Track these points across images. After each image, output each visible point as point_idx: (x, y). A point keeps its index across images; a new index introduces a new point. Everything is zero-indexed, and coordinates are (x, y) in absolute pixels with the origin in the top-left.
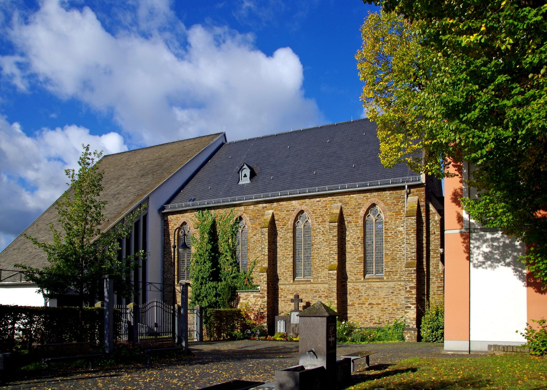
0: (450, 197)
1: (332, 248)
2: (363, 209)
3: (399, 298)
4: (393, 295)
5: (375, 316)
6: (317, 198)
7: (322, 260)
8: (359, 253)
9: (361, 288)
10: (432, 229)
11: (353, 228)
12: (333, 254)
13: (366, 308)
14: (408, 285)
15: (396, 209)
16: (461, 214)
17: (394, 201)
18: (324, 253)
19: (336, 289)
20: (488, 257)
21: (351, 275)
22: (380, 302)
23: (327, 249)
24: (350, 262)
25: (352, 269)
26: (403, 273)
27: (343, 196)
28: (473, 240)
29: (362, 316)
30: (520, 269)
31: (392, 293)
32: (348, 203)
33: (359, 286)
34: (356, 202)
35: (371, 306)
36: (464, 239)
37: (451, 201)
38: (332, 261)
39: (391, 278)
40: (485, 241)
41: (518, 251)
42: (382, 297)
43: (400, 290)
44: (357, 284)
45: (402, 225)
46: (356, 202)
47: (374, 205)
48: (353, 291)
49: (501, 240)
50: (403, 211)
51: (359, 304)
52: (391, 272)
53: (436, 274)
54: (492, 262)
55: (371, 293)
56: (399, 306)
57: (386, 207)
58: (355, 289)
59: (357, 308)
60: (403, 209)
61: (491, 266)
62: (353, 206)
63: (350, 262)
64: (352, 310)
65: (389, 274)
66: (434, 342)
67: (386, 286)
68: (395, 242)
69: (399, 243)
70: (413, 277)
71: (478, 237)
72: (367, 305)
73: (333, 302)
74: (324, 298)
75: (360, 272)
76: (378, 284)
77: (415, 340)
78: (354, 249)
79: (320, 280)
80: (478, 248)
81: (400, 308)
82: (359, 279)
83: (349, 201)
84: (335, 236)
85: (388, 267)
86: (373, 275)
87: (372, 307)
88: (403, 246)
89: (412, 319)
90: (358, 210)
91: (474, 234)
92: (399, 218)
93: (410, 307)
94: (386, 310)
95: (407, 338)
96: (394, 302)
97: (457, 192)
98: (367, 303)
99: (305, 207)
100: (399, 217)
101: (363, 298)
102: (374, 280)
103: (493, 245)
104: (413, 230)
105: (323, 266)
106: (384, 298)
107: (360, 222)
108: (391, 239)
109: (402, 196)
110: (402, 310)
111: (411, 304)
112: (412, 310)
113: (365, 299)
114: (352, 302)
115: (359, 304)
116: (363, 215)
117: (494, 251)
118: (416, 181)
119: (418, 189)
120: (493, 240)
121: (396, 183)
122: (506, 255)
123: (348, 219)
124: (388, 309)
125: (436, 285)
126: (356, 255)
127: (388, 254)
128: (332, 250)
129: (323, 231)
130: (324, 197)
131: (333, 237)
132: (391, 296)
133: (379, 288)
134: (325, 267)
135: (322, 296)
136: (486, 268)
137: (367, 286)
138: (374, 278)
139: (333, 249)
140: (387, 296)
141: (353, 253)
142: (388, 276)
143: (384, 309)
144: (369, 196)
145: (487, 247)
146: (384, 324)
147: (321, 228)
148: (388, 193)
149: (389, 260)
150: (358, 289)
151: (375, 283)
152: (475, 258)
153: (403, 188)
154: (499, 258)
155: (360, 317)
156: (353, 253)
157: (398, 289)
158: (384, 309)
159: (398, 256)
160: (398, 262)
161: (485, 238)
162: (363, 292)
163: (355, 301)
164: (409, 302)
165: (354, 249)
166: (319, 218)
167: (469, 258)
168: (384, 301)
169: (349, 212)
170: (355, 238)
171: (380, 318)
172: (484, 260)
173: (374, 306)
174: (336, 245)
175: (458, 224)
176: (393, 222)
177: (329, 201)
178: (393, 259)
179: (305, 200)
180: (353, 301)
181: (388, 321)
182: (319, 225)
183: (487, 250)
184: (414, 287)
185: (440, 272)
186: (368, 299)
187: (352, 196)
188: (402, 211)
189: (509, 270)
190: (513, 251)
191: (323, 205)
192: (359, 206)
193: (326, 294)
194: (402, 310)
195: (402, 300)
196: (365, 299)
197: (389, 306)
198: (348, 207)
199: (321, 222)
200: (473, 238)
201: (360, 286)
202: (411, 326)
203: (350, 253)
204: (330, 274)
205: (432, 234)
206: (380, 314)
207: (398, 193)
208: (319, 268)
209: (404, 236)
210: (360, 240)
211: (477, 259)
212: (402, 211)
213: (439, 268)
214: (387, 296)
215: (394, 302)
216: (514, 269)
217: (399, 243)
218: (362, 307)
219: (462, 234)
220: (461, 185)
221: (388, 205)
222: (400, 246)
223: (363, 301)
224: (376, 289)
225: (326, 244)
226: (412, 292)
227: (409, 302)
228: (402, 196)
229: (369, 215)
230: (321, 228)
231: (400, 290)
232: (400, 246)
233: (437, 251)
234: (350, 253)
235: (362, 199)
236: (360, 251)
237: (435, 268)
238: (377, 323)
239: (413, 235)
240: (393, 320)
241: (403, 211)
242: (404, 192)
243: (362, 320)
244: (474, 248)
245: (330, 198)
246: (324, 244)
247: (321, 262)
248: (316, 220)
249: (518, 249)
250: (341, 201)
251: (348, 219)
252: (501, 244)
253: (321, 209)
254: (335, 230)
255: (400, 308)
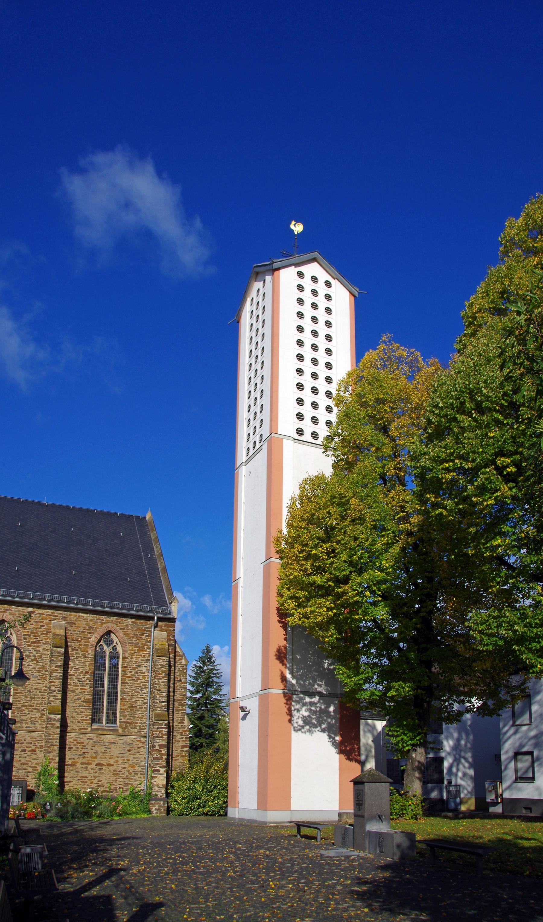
0: (274, 654)
1: (55, 682)
2: (96, 635)
3: (138, 758)
4: (130, 754)
5: (104, 781)
6: (28, 607)
7: (31, 698)
8: (86, 693)
9: (86, 741)
10: (178, 674)
11: (79, 659)
12: (55, 691)
13: (92, 769)
14: (157, 742)
15: (138, 643)
16: (284, 673)
17: (137, 633)
18: (35, 687)
19: (58, 741)
20: (307, 721)
21: (73, 722)
22: (112, 762)
23: (38, 681)
24: (73, 705)
25: (74, 714)
26: (143, 726)
27: (69, 613)
28: (294, 702)
29: (86, 780)
30: (333, 736)
31: (129, 751)
32: (75, 624)
33: (84, 738)
34: (87, 624)
35: (100, 767)
36: (287, 700)
37: (275, 657)
38: (53, 701)
39: (128, 731)
40: (304, 704)
41: (332, 718)
42: (115, 755)
43: (139, 748)
44: (81, 736)
45: (145, 664)
46: (87, 624)
47: (109, 633)
48: (75, 745)
49: (318, 705)
50: (147, 648)
51: (82, 764)
52: (128, 723)
53: (181, 731)
54: (310, 727)
55: (101, 749)
56: (137, 768)
57: (126, 639)
58: (77, 743)
59: (79, 770)
60: (147, 645)
61: (309, 731)
62: (82, 629)
63: (73, 705)
64: (72, 772)
65: (126, 726)
66: (187, 815)
67: (121, 741)
68: (135, 685)
69: (140, 687)
70: (164, 733)
71: (298, 699)
72: (93, 765)
73: (52, 759)
74: (29, 753)
75: (87, 720)
76: (110, 737)
77: (164, 815)
78: (80, 687)
79: (24, 725)
80: (298, 711)
81: (139, 772)
82: (84, 729)
83: (76, 620)
84: (60, 667)
85: (125, 717)
86: (102, 725)
87: (101, 769)
88: (145, 691)
89: (161, 786)
90: (89, 635)
91: (295, 696)
92: (141, 655)
93: (159, 771)
94: (120, 773)
95: (155, 812)
96: (130, 763)
97: (281, 649)
98: (94, 763)
99: (9, 617)
100: (141, 653)
101: (89, 755)
102: (105, 732)
103: (311, 710)
104: (164, 674)
105: (31, 706)
106: (118, 757)
107: (90, 651)
108: (130, 680)
109: (147, 628)
110: (141, 774)
111: (160, 767)
112: (160, 774)
113: (92, 757)
114: (73, 760)
115: (82, 764)
116: (95, 644)
117: (312, 716)
118: (166, 613)
119: (167, 623)
120: (312, 704)
121: (141, 611)
122: (322, 721)
123: (73, 645)
124: (123, 772)
125: (181, 743)
126: (81, 695)
127: (126, 699)
128: (53, 686)
129: (34, 656)
130: (7, 604)
131: (57, 666)
132: (127, 754)
133: (111, 743)
134: (35, 707)
135: (27, 749)
136: (305, 733)
137: (95, 739)
138: (104, 730)
139: (56, 684)
140: (121, 755)
141: (77, 692)
142: (125, 728)
143: (117, 771)
144: (105, 619)
145: (306, 711)
146: (117, 792)
147: (33, 651)
148: (130, 621)
149: (126, 707)
150: (83, 743)
151: (107, 736)
152: (295, 721)
153: (152, 618)
154: (316, 723)
155: (83, 782)
156: (77, 692)
157: (136, 746)
158: (117, 771)
159: (139, 704)
160: (138, 711)
161: (304, 701)
162: (89, 747)
163: (76, 760)
164: (158, 764)
165: (80, 687)
166: (30, 636)
167: (290, 721)
168: (117, 761)
169: (76, 635)
170: (82, 673)
171: (111, 783)
172: (303, 725)
173: (104, 767)
174: (59, 679)
175: (281, 684)
176: (134, 660)
177: (47, 615)
178: (131, 707)
179: (10, 607)
180: (74, 759)
181: (123, 788)
182: (30, 646)
183: (306, 714)
184: (164, 745)
185: (186, 729)
186: (96, 758)
187: (81, 614)
188: (146, 647)
189: (324, 736)
190: (327, 718)
191: (38, 619)
192: (91, 630)
193: (33, 747)
194: (141, 774)
195: (141, 761)
196: (92, 757)
197: (124, 768)
198: (74, 628)
199: (32, 642)
200: (294, 699)
201: (85, 738)
202: (160, 795)
203: (73, 691)
204: (51, 718)
205: (178, 681)
206: (111, 779)
207: (142, 623)
208: (24, 708)
209: (147, 679)
210: (88, 676)
211: (297, 723)
212: (146, 647)
213: (184, 723)
214: (121, 755)
215: (130, 763)
216: (328, 735)
217: (140, 687)
218: (87, 768)
219: (285, 695)
220: (285, 642)
221: (128, 636)
222: (142, 690)
223: (88, 760)
224: (107, 744)
225: (38, 674)
226: (161, 751)
227: (158, 764)
228: (147, 628)
229: (101, 645)
230: (33, 651)
231: (139, 748)
232: (142, 690)
233: (183, 702)
234: (73, 691)
235: (95, 622)
236: (88, 690)
237: (179, 723)
238: (107, 791)
239: (164, 680)
240: (129, 787)
241: (147, 648)
242: (150, 623)
243: (86, 786)
244: (294, 710)
245: (49, 612)
246: (35, 674)
247: (29, 699)
248: (25, 639)
249: (331, 715)
250: (64, 619)
251: (73, 645)
252: (318, 709)
253: (34, 623)
254: (60, 658)
255: (139, 772)
